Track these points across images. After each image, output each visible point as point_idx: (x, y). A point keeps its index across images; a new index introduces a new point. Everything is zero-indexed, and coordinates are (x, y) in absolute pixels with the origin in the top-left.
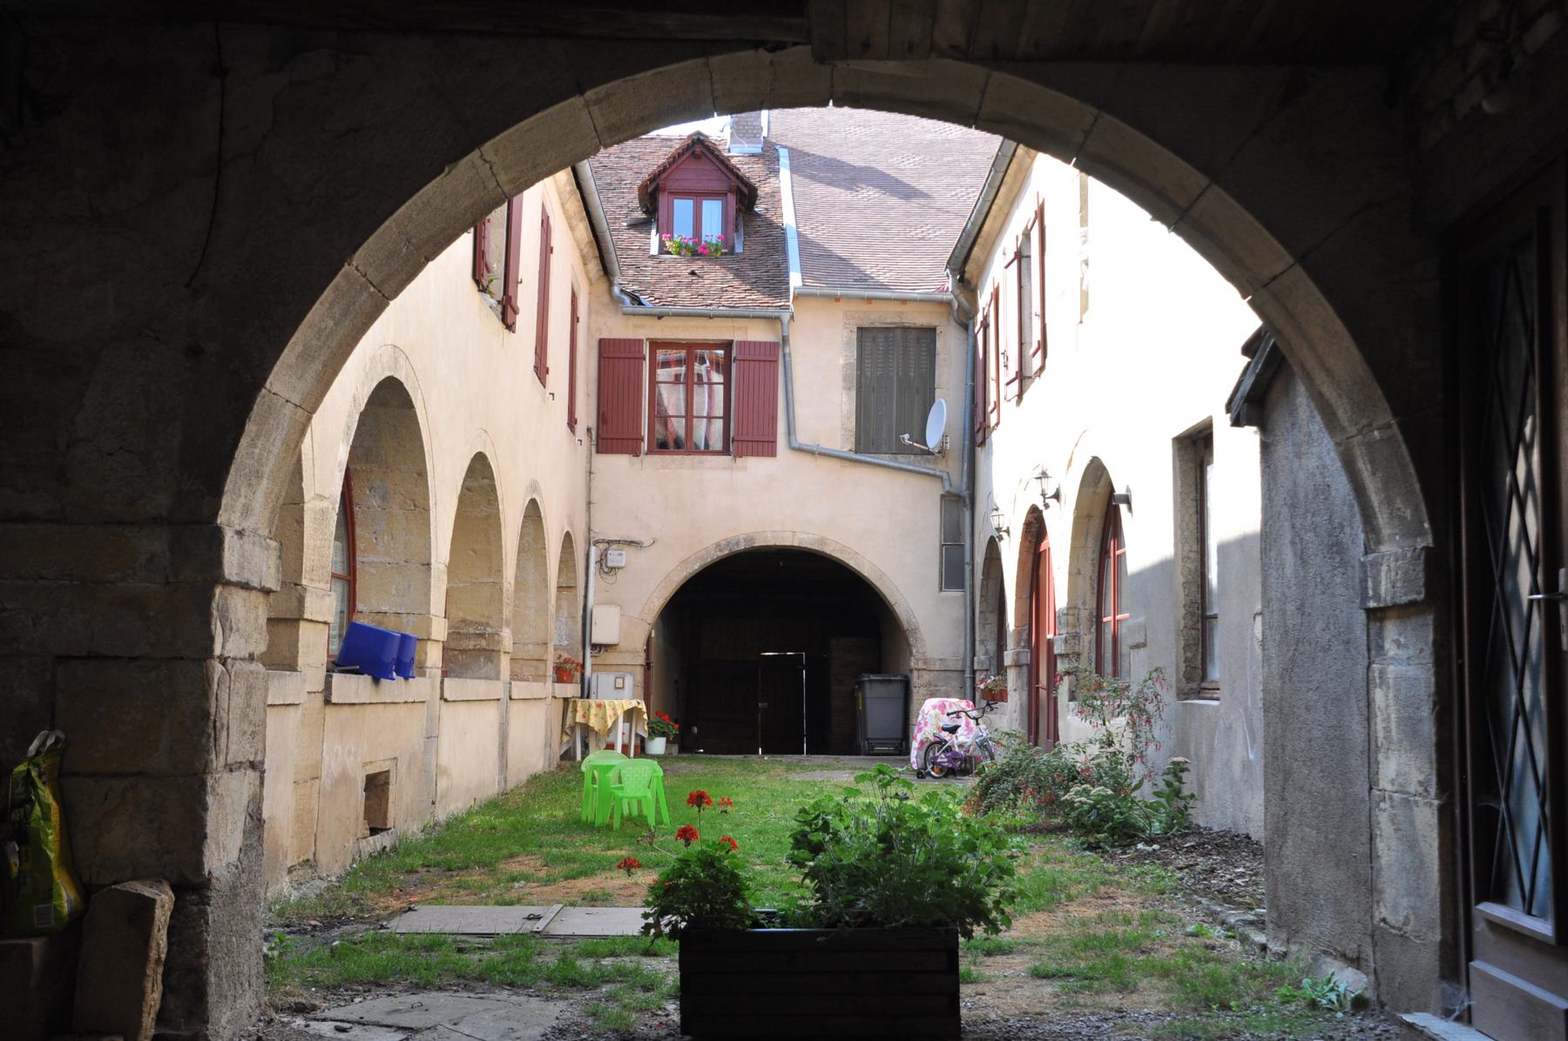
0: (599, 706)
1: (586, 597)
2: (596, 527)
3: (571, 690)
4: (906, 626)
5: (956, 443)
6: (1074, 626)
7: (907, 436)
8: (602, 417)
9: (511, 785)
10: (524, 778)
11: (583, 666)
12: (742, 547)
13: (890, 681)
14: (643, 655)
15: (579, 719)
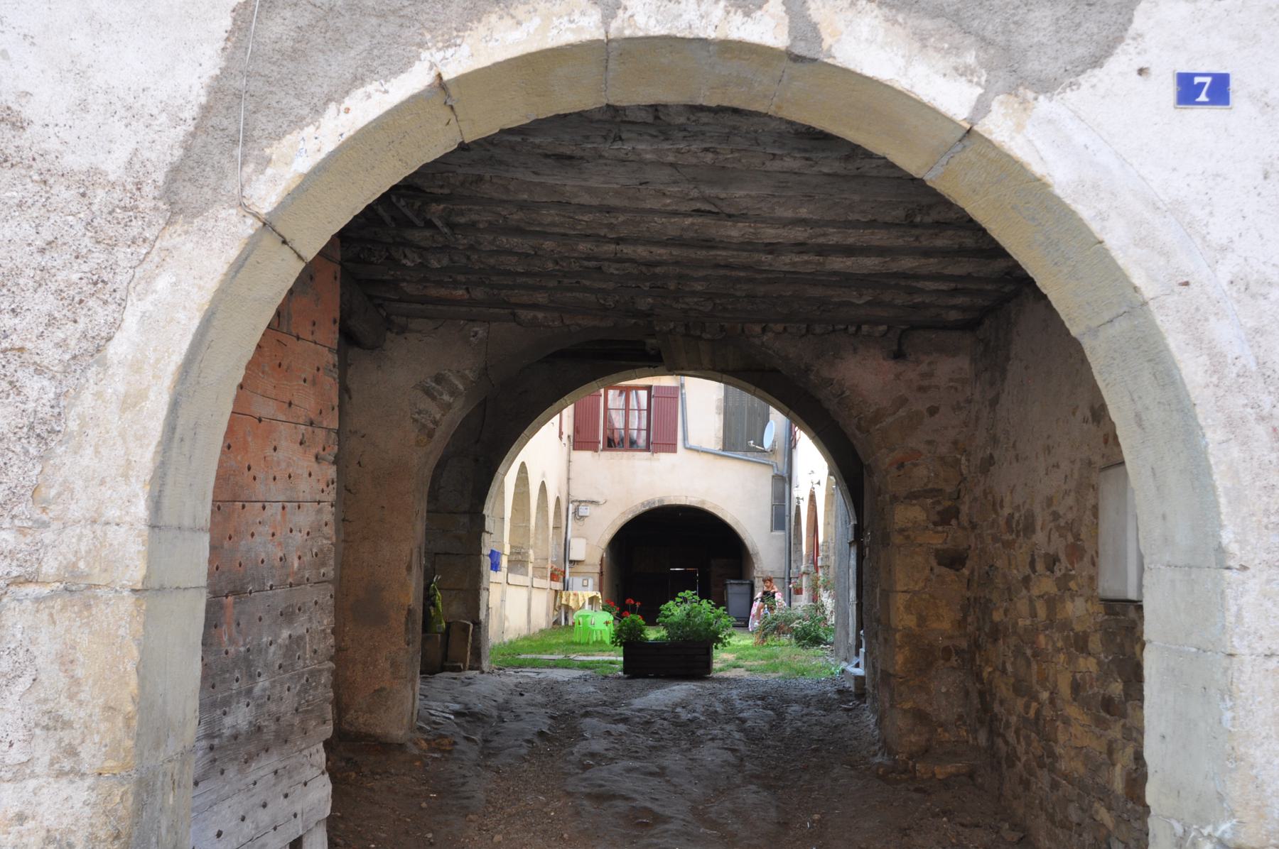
0: (575, 595)
1: (566, 533)
2: (572, 493)
3: (558, 586)
4: (751, 552)
5: (781, 445)
6: (826, 552)
7: (752, 442)
8: (576, 430)
9: (532, 632)
10: (537, 630)
11: (564, 572)
12: (657, 505)
13: (742, 584)
14: (599, 567)
15: (564, 602)
